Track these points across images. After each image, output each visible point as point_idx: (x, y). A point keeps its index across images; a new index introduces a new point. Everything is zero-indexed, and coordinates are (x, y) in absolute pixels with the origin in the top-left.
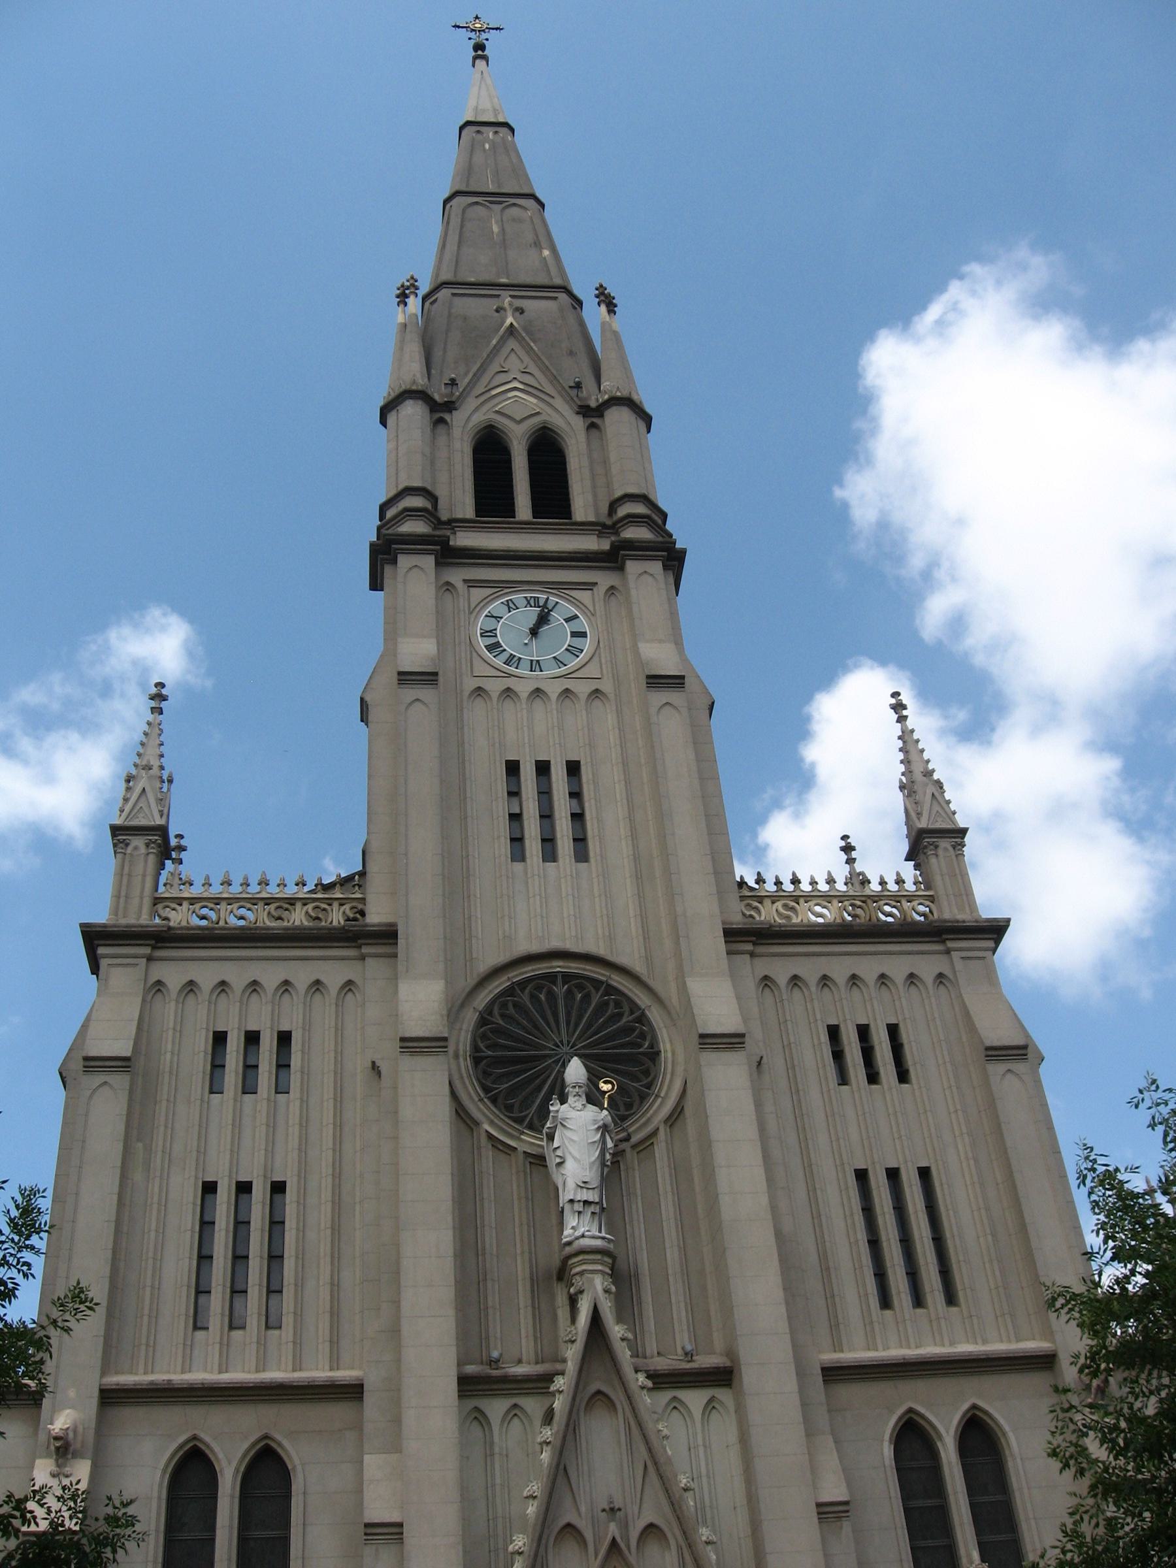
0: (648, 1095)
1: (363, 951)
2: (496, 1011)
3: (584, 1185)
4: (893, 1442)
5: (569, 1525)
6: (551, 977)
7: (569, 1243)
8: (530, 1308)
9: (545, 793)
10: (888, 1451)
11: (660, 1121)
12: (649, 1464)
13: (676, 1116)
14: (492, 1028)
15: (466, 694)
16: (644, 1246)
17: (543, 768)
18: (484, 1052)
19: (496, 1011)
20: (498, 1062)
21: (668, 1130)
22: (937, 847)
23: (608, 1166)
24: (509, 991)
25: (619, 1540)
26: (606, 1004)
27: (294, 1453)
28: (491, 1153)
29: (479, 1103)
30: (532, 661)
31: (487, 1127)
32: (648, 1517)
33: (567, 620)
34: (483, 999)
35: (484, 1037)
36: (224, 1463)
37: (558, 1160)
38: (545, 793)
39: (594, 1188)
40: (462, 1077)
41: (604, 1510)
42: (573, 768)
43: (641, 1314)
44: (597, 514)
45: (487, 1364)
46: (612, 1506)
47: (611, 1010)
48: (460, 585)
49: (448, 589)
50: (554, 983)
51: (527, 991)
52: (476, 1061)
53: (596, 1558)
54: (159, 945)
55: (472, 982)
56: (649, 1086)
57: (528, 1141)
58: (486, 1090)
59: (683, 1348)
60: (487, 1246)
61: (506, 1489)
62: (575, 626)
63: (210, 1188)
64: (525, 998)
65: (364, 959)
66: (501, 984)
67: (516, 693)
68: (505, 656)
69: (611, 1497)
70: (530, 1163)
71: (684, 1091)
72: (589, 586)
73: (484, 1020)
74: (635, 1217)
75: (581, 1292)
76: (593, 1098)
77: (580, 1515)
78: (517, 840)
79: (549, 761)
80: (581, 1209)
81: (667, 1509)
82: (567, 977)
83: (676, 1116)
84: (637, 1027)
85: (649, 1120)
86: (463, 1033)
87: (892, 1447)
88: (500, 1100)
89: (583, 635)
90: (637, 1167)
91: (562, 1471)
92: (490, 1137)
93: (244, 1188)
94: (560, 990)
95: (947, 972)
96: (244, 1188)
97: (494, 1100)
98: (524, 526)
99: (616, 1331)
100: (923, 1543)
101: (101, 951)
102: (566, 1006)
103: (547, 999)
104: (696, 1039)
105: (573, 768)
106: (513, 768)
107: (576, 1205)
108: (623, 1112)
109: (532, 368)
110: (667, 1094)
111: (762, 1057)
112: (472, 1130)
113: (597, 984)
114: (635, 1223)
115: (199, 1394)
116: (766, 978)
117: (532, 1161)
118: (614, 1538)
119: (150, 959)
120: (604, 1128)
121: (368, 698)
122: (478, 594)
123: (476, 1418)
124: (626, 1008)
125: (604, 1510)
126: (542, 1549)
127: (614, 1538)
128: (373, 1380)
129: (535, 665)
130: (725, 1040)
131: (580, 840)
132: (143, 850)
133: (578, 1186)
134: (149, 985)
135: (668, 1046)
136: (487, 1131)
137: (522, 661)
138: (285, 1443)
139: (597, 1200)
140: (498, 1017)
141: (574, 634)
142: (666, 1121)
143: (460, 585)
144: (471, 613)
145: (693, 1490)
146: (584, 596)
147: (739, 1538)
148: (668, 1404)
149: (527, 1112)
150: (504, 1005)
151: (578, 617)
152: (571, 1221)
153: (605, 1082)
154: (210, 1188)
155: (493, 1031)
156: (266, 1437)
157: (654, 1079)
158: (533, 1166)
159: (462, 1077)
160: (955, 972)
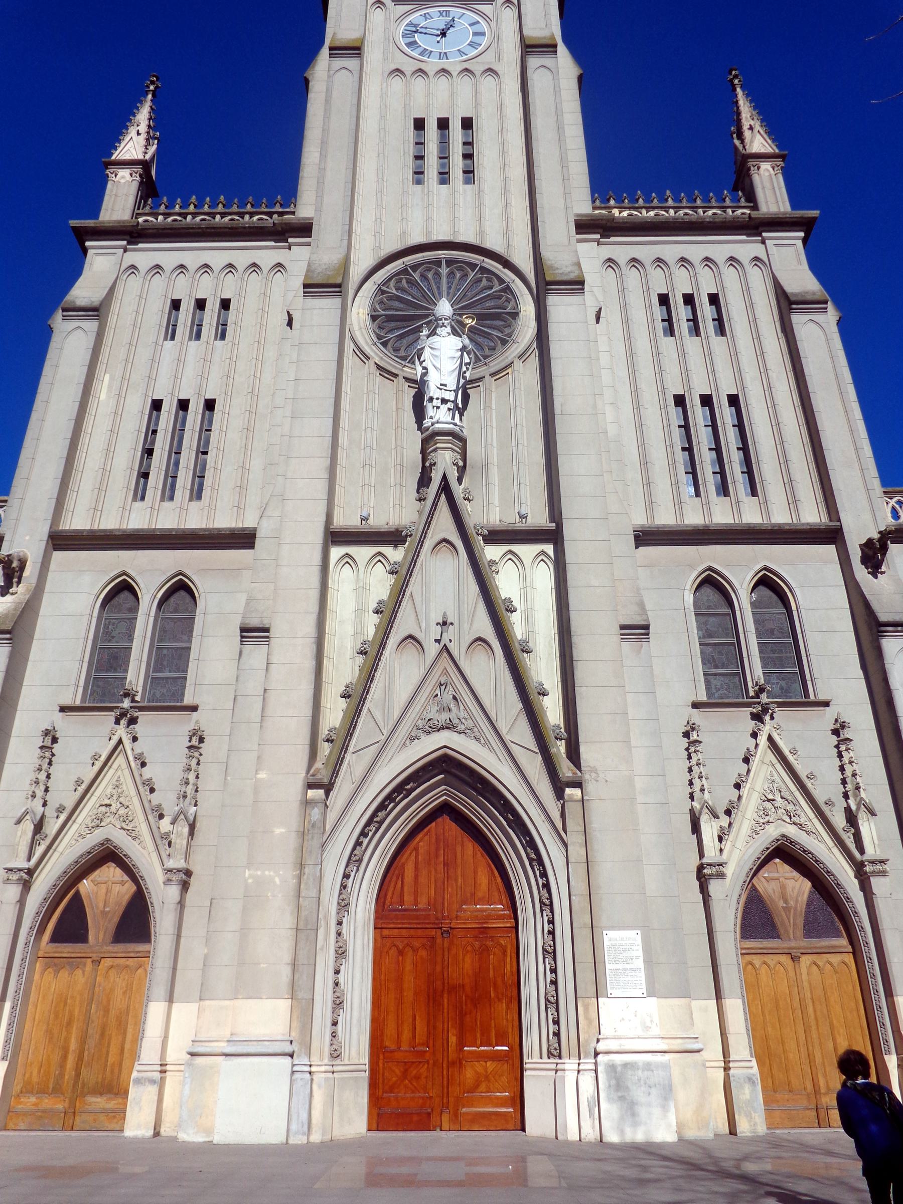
6: (438, 263)
9: (444, 143)
11: (515, 357)
14: (388, 296)
17: (443, 124)
18: (379, 311)
20: (390, 319)
22: (759, 168)
24: (404, 271)
27: (201, 585)
29: (372, 346)
30: (440, 53)
33: (471, 25)
38: (444, 143)
42: (467, 124)
45: (812, 928)
46: (445, 620)
47: (484, 282)
49: (379, 7)
50: (440, 266)
58: (379, 337)
62: (477, 28)
63: (157, 405)
64: (416, 276)
65: (290, 249)
68: (420, 50)
69: (445, 614)
70: (409, 386)
79: (448, 119)
80: (439, 405)
82: (450, 262)
84: (503, 296)
88: (390, 345)
89: (483, 34)
93: (183, 405)
96: (183, 405)
97: (385, 344)
101: (88, 244)
102: (448, 283)
105: (467, 124)
106: (419, 124)
111: (600, 309)
113: (473, 266)
116: (610, 260)
120: (464, 349)
129: (444, 55)
134: (123, 268)
137: (432, 54)
139: (452, 398)
140: (394, 289)
141: (475, 34)
151: (480, 23)
154: (157, 405)
157: (513, 332)
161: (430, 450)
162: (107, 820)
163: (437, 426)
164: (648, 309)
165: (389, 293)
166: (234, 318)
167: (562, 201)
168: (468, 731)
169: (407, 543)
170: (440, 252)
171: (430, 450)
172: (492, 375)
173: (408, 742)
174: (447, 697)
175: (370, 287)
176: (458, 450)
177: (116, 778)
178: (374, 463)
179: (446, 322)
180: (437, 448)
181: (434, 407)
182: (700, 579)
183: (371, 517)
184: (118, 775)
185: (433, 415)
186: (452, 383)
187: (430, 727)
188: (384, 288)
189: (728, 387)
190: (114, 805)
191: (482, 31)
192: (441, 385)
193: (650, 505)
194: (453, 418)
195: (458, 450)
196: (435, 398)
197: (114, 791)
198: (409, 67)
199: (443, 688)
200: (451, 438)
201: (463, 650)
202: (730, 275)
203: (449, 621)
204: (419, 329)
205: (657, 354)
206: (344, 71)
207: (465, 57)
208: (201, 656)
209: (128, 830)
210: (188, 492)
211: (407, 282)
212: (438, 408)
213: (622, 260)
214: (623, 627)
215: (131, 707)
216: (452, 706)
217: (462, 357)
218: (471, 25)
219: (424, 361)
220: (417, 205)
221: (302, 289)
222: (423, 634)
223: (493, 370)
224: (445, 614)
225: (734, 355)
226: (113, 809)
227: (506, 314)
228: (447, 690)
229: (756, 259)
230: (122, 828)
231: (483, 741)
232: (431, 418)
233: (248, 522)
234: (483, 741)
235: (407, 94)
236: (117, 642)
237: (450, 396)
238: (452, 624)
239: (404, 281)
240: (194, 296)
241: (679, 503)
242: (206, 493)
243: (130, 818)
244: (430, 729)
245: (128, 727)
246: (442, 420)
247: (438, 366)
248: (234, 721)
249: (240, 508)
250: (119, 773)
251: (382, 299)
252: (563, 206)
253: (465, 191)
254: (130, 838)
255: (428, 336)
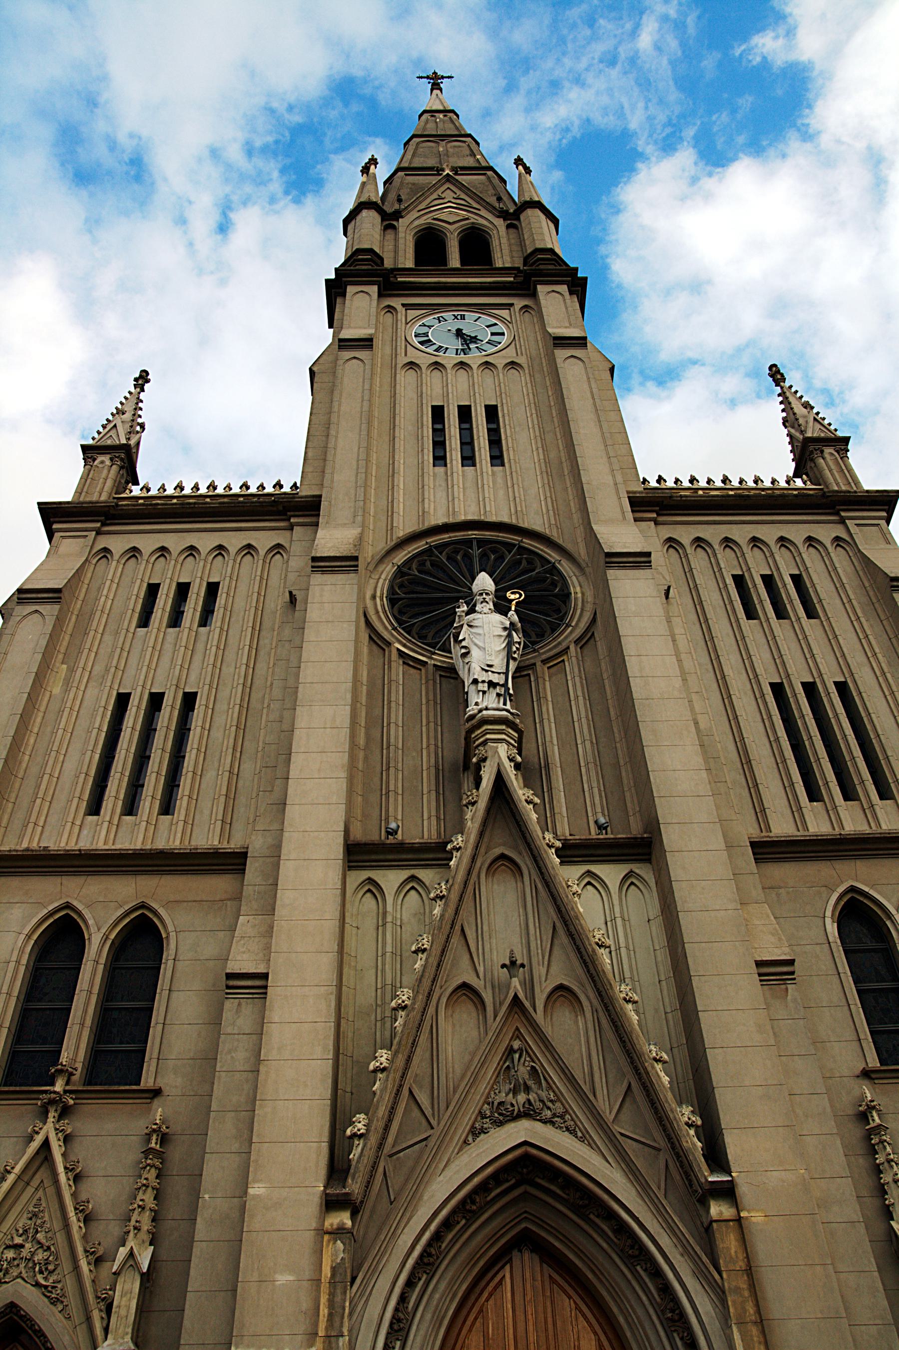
0: (559, 625)
1: (292, 520)
2: (414, 566)
3: (488, 668)
4: (836, 919)
5: (465, 986)
6: (468, 542)
7: (473, 717)
8: (433, 794)
10: (832, 929)
12: (558, 925)
13: (586, 640)
15: (399, 366)
16: (555, 742)
18: (398, 594)
19: (414, 566)
21: (579, 650)
23: (515, 659)
24: (428, 551)
25: (521, 995)
26: (519, 562)
28: (401, 668)
30: (457, 350)
31: (398, 645)
32: (559, 977)
34: (401, 557)
35: (401, 586)
36: (93, 929)
37: (463, 651)
39: (499, 673)
40: (377, 612)
41: (504, 966)
43: (550, 789)
44: (513, 262)
48: (399, 308)
51: (444, 553)
52: (392, 601)
53: (495, 1019)
54: (108, 522)
55: (391, 544)
56: (562, 619)
57: (439, 659)
59: (596, 822)
60: (392, 740)
61: (398, 958)
62: (494, 329)
65: (292, 529)
66: (420, 546)
67: (443, 366)
69: (512, 952)
70: (441, 676)
71: (594, 620)
72: (509, 306)
73: (400, 572)
74: (545, 716)
75: (484, 760)
76: (501, 607)
77: (478, 976)
78: (439, 444)
80: (486, 689)
81: (580, 971)
82: (481, 542)
83: (586, 640)
84: (548, 578)
85: (559, 643)
86: (381, 581)
87: (835, 925)
89: (503, 334)
90: (547, 679)
91: (459, 933)
92: (401, 654)
93: (156, 700)
94: (476, 552)
95: (844, 536)
98: (455, 272)
99: (521, 793)
100: (881, 1027)
101: (55, 526)
103: (463, 558)
104: (602, 559)
107: (480, 685)
108: (534, 638)
109: (463, 196)
110: (577, 624)
111: (669, 587)
112: (384, 650)
113: (509, 546)
114: (546, 722)
115: (76, 863)
116: (670, 539)
117: (442, 674)
118: (516, 996)
119: (99, 533)
121: (315, 369)
122: (412, 314)
123: (369, 891)
124: (538, 563)
125: (504, 966)
126: (431, 1010)
127: (516, 996)
128: (257, 845)
130: (631, 559)
131: (495, 441)
132: (108, 463)
133: (483, 669)
134: (94, 551)
135: (578, 589)
136: (398, 649)
138: (162, 912)
139: (502, 682)
142: (576, 642)
143: (399, 308)
144: (407, 324)
145: (609, 947)
146: (504, 313)
147: (666, 1013)
148: (581, 878)
149: (437, 640)
150: (422, 564)
152: (474, 698)
153: (512, 593)
155: (411, 582)
156: (143, 906)
158: (443, 679)
159: (377, 612)
160: (851, 535)
161: (477, 743)
162: (14, 1272)
163: (485, 712)
164: (722, 590)
165: (410, 575)
166: (223, 602)
167: (610, 478)
168: (556, 1119)
169: (454, 859)
170: (470, 533)
171: (477, 743)
172: (544, 662)
173: (470, 1139)
174: (523, 1072)
175: (388, 571)
176: (513, 742)
177: (34, 1201)
178: (400, 765)
179: (488, 598)
180: (487, 739)
181: (479, 691)
182: (840, 907)
183: (400, 832)
184: (37, 1197)
185: (479, 701)
186: (499, 663)
187: (500, 1114)
188: (405, 570)
189: (831, 676)
190: (28, 1245)
191: (500, 331)
192: (489, 666)
193: (761, 813)
194: (505, 704)
195: (513, 742)
196: (480, 680)
197: (29, 1222)
198: (424, 361)
199: (517, 1056)
200: (504, 727)
201: (540, 1005)
202: (810, 557)
203: (519, 962)
204: (457, 599)
205: (740, 640)
206: (354, 361)
207: (484, 353)
208: (168, 1018)
209: (46, 1287)
210: (157, 804)
211: (432, 565)
212: (484, 692)
213: (686, 541)
214: (759, 964)
215: (65, 1092)
216: (530, 1083)
217: (509, 636)
218: (488, 327)
219: (464, 639)
220: (440, 486)
221: (310, 563)
222: (482, 982)
223: (544, 657)
224: (512, 952)
225: (832, 638)
226: (25, 1253)
227: (553, 596)
228: (522, 1060)
229: (837, 539)
230: (37, 1285)
231: (580, 1134)
232: (477, 704)
233: (235, 844)
234: (580, 1134)
235: (420, 385)
236: (50, 1001)
237: (495, 678)
238: (523, 966)
239: (428, 564)
240: (175, 580)
241: (797, 811)
242: (182, 803)
243: (51, 1267)
244: (501, 1118)
245: (58, 1121)
246: (490, 706)
247: (481, 644)
248: (251, 1113)
249: (227, 824)
250: (40, 1193)
251: (403, 581)
252: (612, 483)
253: (493, 474)
254: (46, 1300)
255: (468, 614)
